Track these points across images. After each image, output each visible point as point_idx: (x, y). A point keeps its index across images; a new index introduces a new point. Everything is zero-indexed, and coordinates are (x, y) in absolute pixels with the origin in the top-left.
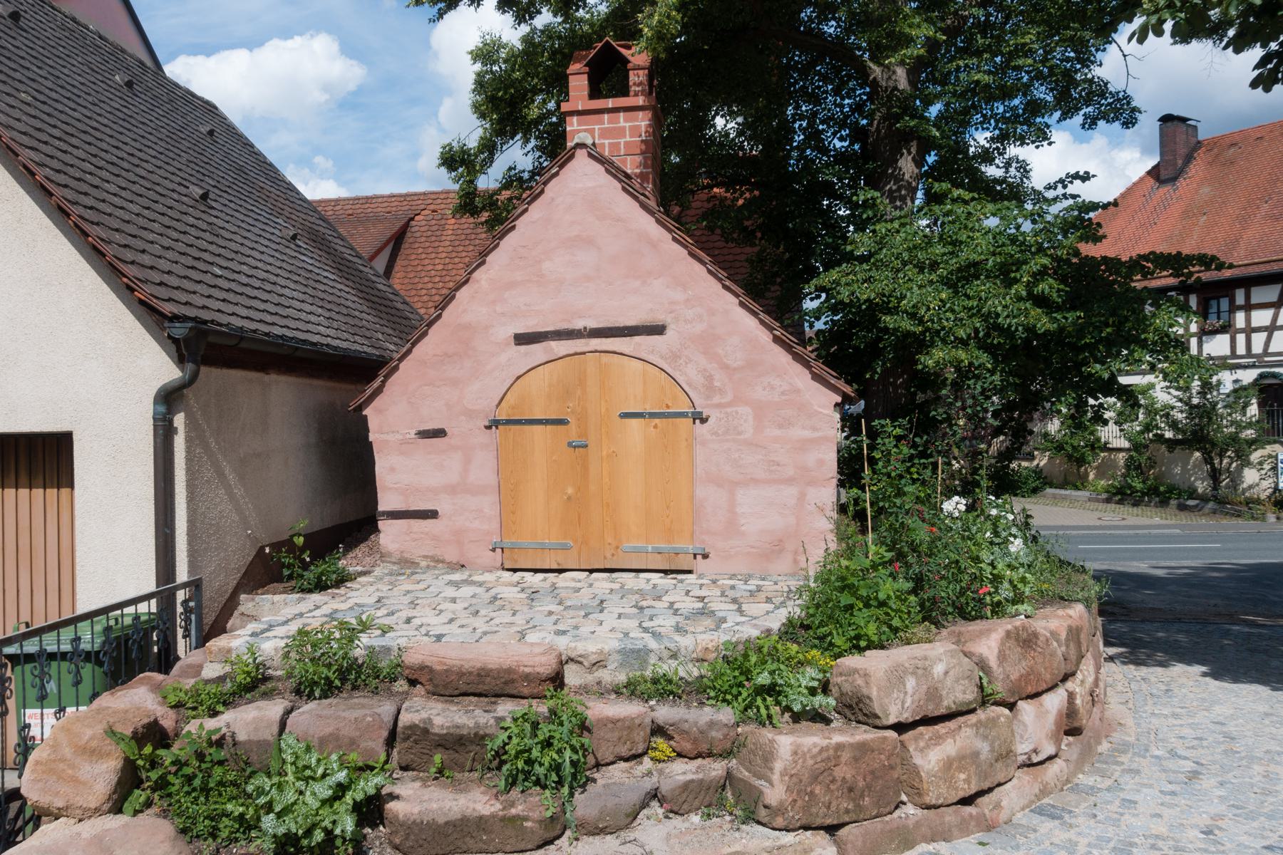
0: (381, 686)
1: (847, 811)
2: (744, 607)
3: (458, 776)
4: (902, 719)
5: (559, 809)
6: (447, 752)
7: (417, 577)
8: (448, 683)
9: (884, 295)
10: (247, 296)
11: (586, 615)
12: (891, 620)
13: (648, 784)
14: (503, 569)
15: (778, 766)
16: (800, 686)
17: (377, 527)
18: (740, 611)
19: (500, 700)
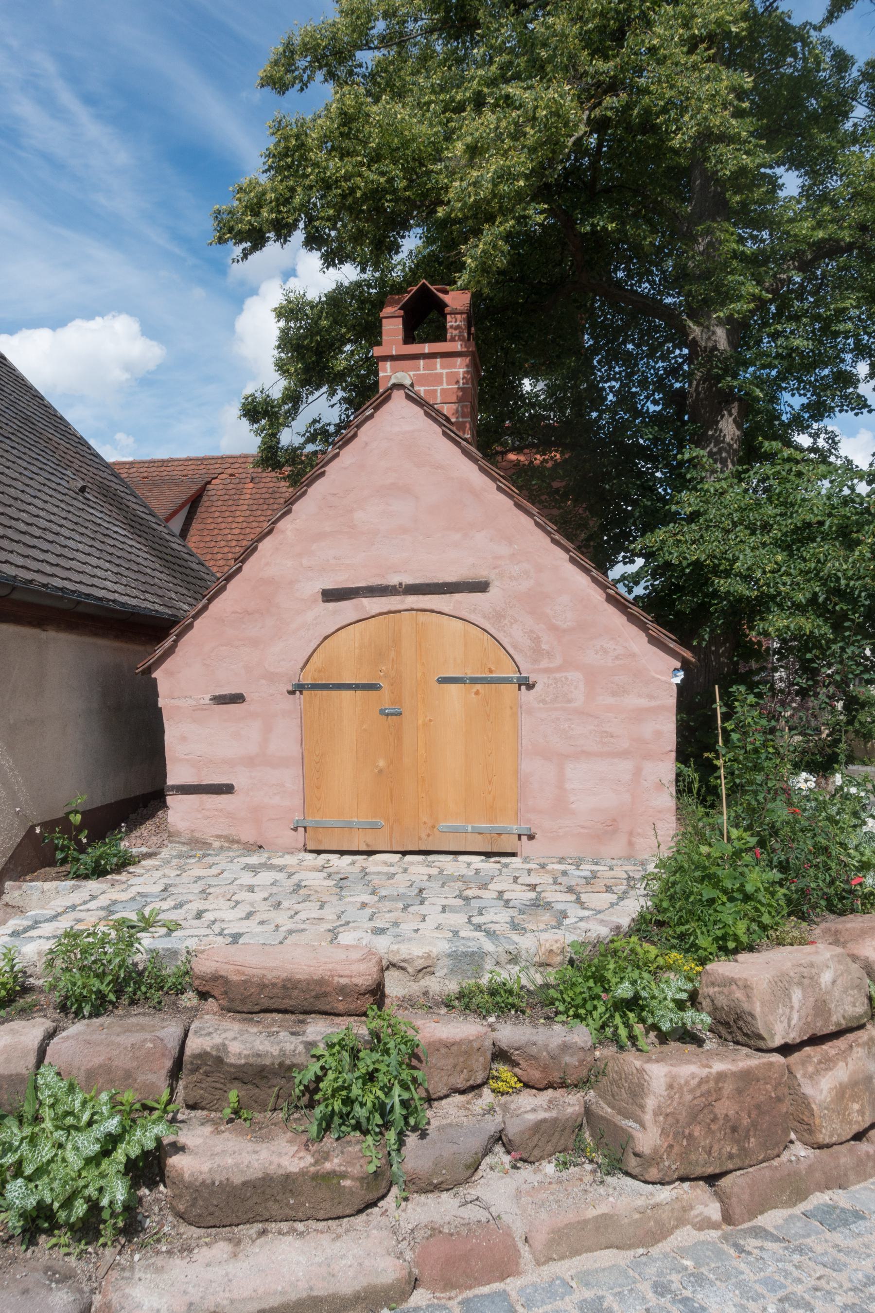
0: (166, 1000)
1: (731, 1156)
2: (584, 898)
3: (258, 1116)
4: (789, 1041)
5: (383, 1161)
6: (245, 1087)
7: (209, 860)
8: (246, 998)
9: (715, 557)
10: (24, 544)
11: (405, 908)
12: (759, 917)
13: (492, 1125)
14: (306, 850)
15: (651, 1103)
16: (665, 999)
17: (165, 802)
18: (578, 901)
19: (309, 1018)
